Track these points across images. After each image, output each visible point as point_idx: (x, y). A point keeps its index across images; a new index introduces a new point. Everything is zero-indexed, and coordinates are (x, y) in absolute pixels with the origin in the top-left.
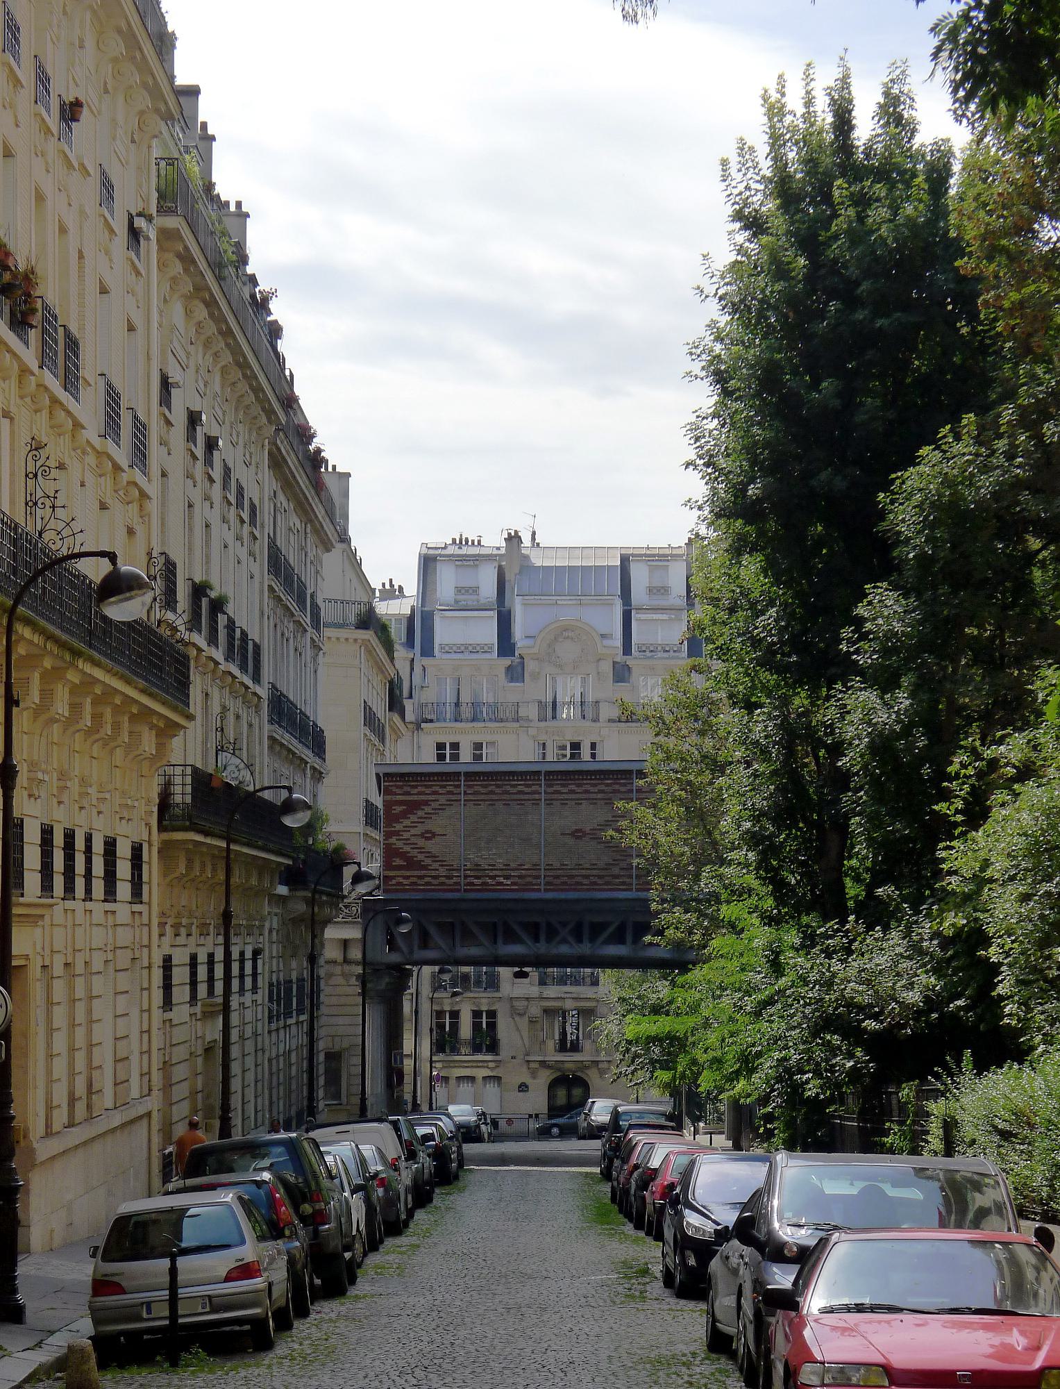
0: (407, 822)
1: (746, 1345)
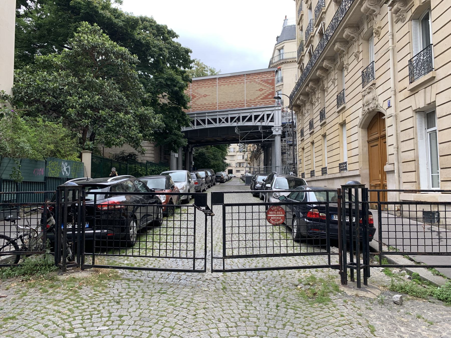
0: (268, 93)
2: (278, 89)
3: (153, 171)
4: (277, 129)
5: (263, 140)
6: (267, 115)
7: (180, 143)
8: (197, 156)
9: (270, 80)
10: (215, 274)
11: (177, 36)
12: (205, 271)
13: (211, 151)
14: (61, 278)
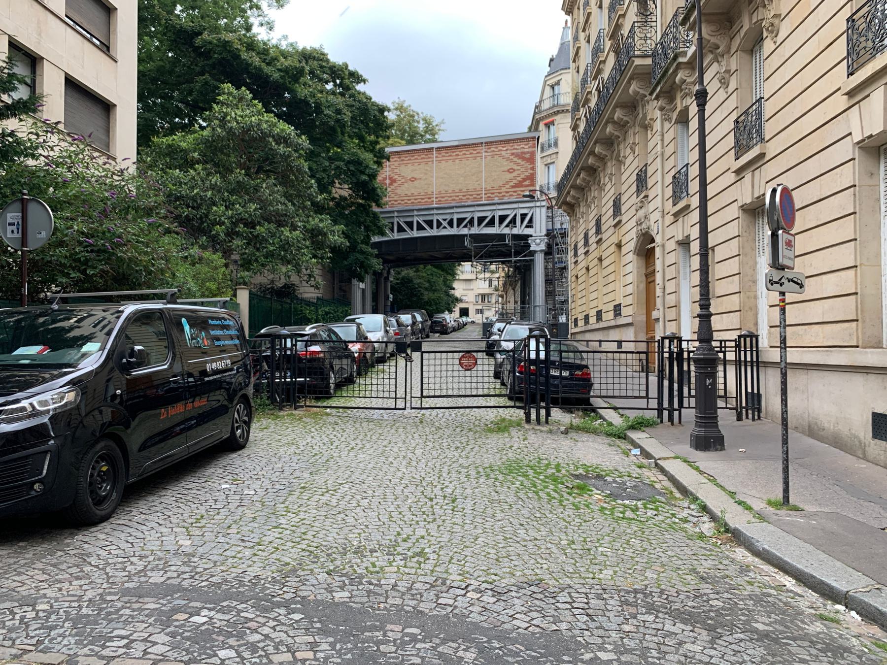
0: (523, 176)
2: (549, 161)
3: (327, 313)
4: (538, 241)
5: (513, 259)
6: (522, 215)
7: (370, 266)
8: (397, 284)
9: (528, 153)
10: (413, 411)
11: (364, 81)
12: (405, 409)
13: (425, 275)
14: (282, 413)
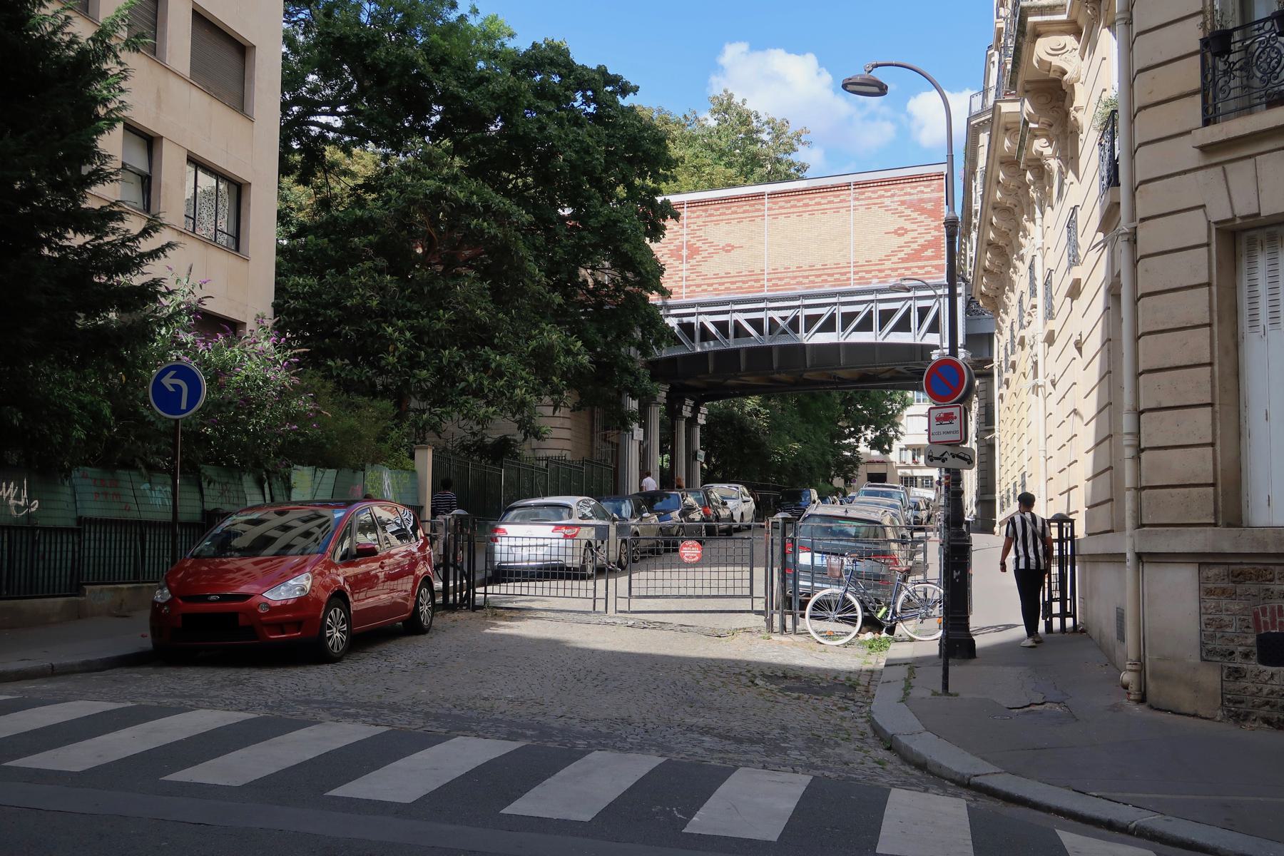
0: (921, 241)
1: (519, 613)
